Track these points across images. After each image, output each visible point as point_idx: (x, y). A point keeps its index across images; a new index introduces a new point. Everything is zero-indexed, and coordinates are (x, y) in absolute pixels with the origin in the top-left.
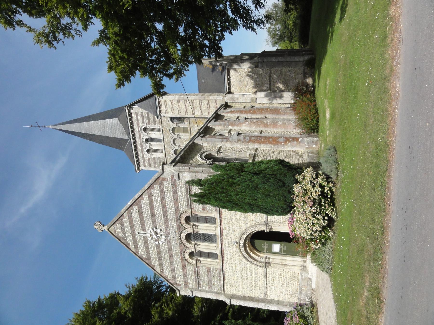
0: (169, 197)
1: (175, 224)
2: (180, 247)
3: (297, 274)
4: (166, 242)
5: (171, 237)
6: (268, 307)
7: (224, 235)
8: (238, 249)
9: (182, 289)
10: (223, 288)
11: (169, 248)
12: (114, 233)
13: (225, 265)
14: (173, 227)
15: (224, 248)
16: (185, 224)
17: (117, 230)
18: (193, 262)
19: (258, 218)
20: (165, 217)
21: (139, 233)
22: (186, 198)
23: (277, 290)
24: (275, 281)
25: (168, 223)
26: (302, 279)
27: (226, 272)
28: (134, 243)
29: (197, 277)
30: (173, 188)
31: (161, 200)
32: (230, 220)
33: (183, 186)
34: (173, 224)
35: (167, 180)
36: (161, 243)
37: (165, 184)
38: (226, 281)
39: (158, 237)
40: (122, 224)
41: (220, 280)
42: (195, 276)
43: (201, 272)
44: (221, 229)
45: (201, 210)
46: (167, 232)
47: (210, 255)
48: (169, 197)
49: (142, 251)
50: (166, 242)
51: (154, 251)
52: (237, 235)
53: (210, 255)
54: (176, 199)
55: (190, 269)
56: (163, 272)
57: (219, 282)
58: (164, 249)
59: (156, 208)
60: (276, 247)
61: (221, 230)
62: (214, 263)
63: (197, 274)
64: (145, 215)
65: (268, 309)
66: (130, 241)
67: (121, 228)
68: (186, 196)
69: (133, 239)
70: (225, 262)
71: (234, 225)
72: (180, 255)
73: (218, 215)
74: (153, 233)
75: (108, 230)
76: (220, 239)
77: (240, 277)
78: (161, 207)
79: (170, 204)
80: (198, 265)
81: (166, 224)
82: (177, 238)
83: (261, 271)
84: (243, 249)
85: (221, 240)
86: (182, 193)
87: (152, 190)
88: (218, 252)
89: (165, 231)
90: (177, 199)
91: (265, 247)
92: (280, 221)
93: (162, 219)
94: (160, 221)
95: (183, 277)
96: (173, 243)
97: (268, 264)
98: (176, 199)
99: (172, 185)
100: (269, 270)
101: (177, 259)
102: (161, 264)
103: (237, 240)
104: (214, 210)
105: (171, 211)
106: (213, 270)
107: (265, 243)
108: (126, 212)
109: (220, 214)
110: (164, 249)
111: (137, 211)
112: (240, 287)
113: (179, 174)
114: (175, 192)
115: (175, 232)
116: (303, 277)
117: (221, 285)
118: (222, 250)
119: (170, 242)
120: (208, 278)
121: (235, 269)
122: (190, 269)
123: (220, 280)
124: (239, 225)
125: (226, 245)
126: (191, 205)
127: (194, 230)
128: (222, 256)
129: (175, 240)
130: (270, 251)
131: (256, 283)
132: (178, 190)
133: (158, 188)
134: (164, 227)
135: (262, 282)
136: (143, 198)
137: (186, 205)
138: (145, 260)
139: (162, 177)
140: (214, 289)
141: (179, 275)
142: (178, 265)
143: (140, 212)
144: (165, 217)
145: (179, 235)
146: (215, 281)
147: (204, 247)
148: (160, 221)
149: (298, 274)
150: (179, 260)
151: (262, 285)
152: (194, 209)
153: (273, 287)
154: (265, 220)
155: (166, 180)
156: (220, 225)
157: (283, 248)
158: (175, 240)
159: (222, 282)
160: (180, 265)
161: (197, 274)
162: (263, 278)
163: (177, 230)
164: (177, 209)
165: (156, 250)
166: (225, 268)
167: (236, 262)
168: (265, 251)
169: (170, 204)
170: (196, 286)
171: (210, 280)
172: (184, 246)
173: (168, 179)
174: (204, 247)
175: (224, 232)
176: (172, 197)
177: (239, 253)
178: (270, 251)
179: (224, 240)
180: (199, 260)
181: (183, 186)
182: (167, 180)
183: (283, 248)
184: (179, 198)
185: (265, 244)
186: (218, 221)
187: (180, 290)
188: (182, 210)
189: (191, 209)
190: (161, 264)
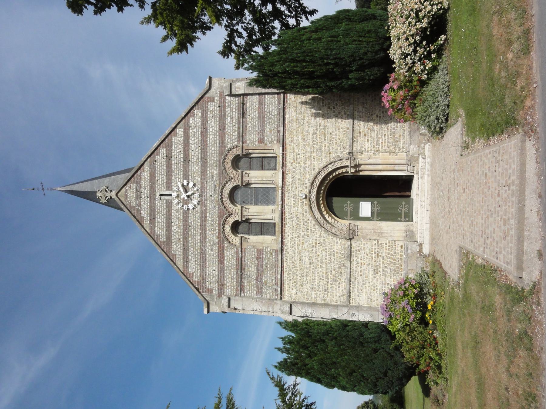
0: (213, 127)
1: (216, 172)
2: (220, 213)
3: (400, 249)
4: (199, 206)
5: (208, 195)
6: (353, 315)
7: (287, 184)
8: (307, 207)
9: (213, 300)
10: (279, 289)
11: (202, 217)
12: (123, 201)
13: (285, 241)
14: (213, 176)
15: (286, 209)
16: (230, 206)
17: (129, 195)
18: (235, 240)
19: (339, 148)
20: (204, 160)
21: (161, 195)
22: (237, 126)
23: (367, 285)
24: (365, 267)
25: (206, 171)
26: (407, 255)
27: (287, 256)
28: (150, 216)
29: (239, 272)
30: (220, 111)
31: (202, 132)
32: (298, 157)
33: (234, 107)
34: (213, 171)
35: (214, 101)
36: (191, 206)
37: (211, 106)
38: (285, 274)
39: (188, 196)
40: (138, 183)
41: (276, 273)
42: (237, 269)
43: (247, 261)
44: (283, 172)
45: (257, 143)
46: (204, 184)
47: (265, 228)
48: (213, 127)
49: (160, 231)
50: (199, 206)
51: (179, 227)
52: (306, 181)
53: (265, 228)
54: (222, 128)
55: (230, 254)
56: (186, 267)
57: (273, 278)
58: (194, 219)
59: (192, 147)
60: (365, 207)
61: (283, 175)
62: (268, 242)
63: (241, 265)
64: (174, 161)
65: (353, 319)
66: (145, 213)
67: (137, 190)
68: (237, 121)
69: (150, 208)
70: (286, 235)
71: (302, 164)
72: (217, 228)
73: (281, 148)
74: (181, 189)
75: (117, 195)
76: (280, 191)
77: (308, 263)
78: (200, 145)
79: (213, 138)
80: (245, 245)
81: (204, 173)
82: (216, 197)
83: (344, 243)
84: (314, 205)
85: (282, 193)
86: (232, 118)
87: (191, 119)
88: (276, 219)
89: (199, 186)
90: (224, 128)
91: (349, 209)
92: (371, 150)
93: (197, 165)
94: (195, 168)
95: (217, 273)
96: (210, 206)
97: (351, 235)
98: (222, 128)
99: (219, 106)
100: (355, 244)
101: (213, 236)
102: (185, 250)
103: (307, 192)
104: (275, 142)
105: (213, 149)
106: (267, 253)
107: (349, 202)
108: (149, 160)
109: (283, 147)
110: (194, 219)
111: (165, 155)
112: (308, 285)
113: (231, 84)
114: (222, 117)
115: (215, 186)
116: (409, 251)
117: (276, 284)
118: (282, 213)
119: (205, 206)
120: (258, 270)
121: (300, 248)
122: (230, 254)
123: (276, 273)
124: (309, 163)
125: (289, 201)
126: (243, 136)
127: (244, 178)
128: (282, 223)
129: (212, 201)
130: (356, 216)
131: (334, 273)
132: (227, 113)
133: (200, 114)
134: (199, 179)
135: (343, 270)
136: (176, 133)
137: (236, 136)
138: (163, 246)
139: (207, 95)
140: (266, 294)
141: (212, 270)
142: (212, 250)
143: (169, 157)
144: (204, 160)
145: (220, 191)
146: (269, 277)
147: (256, 176)
148: (195, 168)
149: (401, 247)
150: (214, 238)
151: (344, 278)
152: (246, 142)
153: (360, 279)
154: (348, 151)
155: (212, 100)
156: (283, 166)
157: (376, 209)
158: (212, 201)
159: (279, 277)
160: (216, 249)
161: (241, 265)
162: (345, 262)
163: (218, 182)
164: (222, 143)
165: (181, 224)
166: (285, 247)
167: (303, 233)
168: (348, 218)
169: (213, 138)
170: (237, 290)
171: (260, 275)
172: (225, 210)
173: (216, 98)
174: (255, 212)
175: (288, 178)
176: (218, 127)
177: (309, 216)
178: (356, 216)
179: (287, 194)
180: (246, 238)
181: (234, 107)
182: (214, 101)
183: (376, 209)
184: (226, 127)
185: (347, 203)
186: (278, 229)
187: (210, 302)
188: (229, 146)
189: (243, 143)
190: (185, 250)
